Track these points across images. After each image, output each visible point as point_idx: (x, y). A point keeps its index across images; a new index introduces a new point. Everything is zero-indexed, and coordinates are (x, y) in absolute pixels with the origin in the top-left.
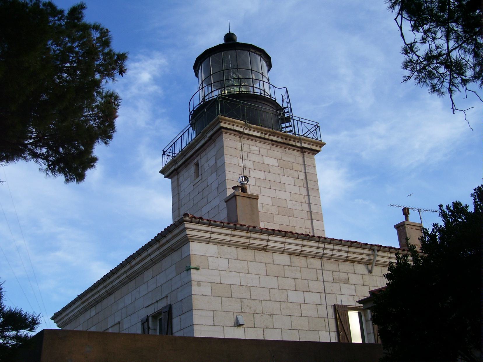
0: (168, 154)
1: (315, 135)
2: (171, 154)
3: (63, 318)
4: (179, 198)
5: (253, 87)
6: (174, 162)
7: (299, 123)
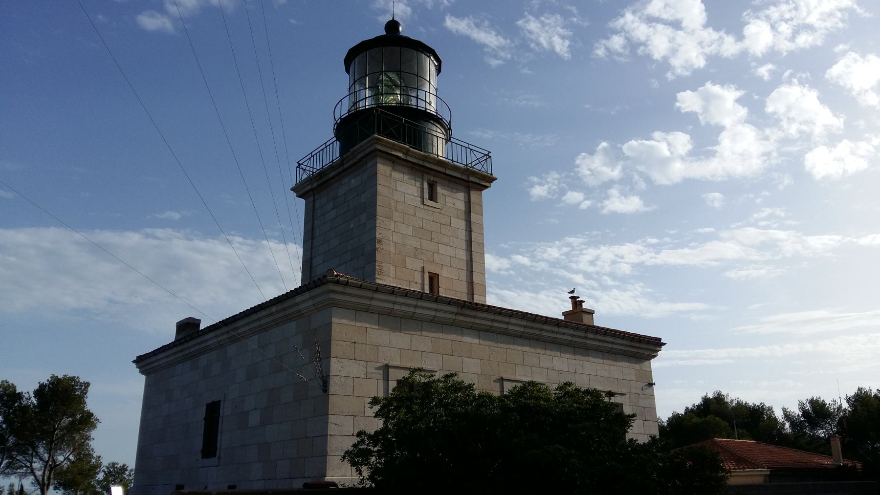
0: (304, 167)
1: (485, 166)
2: (308, 168)
3: (189, 348)
4: (312, 243)
5: (417, 98)
6: (310, 180)
7: (468, 150)
